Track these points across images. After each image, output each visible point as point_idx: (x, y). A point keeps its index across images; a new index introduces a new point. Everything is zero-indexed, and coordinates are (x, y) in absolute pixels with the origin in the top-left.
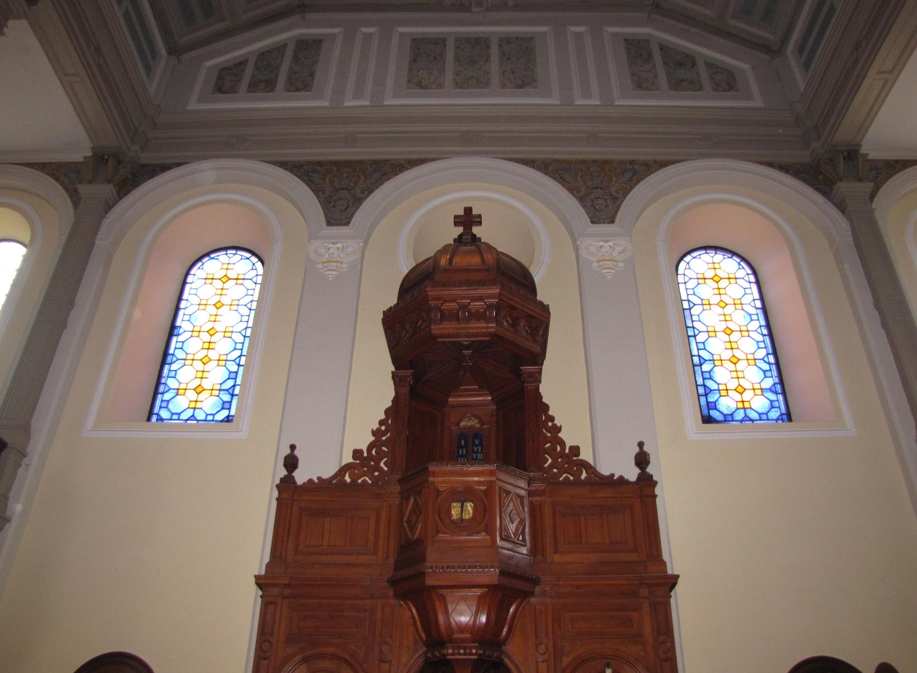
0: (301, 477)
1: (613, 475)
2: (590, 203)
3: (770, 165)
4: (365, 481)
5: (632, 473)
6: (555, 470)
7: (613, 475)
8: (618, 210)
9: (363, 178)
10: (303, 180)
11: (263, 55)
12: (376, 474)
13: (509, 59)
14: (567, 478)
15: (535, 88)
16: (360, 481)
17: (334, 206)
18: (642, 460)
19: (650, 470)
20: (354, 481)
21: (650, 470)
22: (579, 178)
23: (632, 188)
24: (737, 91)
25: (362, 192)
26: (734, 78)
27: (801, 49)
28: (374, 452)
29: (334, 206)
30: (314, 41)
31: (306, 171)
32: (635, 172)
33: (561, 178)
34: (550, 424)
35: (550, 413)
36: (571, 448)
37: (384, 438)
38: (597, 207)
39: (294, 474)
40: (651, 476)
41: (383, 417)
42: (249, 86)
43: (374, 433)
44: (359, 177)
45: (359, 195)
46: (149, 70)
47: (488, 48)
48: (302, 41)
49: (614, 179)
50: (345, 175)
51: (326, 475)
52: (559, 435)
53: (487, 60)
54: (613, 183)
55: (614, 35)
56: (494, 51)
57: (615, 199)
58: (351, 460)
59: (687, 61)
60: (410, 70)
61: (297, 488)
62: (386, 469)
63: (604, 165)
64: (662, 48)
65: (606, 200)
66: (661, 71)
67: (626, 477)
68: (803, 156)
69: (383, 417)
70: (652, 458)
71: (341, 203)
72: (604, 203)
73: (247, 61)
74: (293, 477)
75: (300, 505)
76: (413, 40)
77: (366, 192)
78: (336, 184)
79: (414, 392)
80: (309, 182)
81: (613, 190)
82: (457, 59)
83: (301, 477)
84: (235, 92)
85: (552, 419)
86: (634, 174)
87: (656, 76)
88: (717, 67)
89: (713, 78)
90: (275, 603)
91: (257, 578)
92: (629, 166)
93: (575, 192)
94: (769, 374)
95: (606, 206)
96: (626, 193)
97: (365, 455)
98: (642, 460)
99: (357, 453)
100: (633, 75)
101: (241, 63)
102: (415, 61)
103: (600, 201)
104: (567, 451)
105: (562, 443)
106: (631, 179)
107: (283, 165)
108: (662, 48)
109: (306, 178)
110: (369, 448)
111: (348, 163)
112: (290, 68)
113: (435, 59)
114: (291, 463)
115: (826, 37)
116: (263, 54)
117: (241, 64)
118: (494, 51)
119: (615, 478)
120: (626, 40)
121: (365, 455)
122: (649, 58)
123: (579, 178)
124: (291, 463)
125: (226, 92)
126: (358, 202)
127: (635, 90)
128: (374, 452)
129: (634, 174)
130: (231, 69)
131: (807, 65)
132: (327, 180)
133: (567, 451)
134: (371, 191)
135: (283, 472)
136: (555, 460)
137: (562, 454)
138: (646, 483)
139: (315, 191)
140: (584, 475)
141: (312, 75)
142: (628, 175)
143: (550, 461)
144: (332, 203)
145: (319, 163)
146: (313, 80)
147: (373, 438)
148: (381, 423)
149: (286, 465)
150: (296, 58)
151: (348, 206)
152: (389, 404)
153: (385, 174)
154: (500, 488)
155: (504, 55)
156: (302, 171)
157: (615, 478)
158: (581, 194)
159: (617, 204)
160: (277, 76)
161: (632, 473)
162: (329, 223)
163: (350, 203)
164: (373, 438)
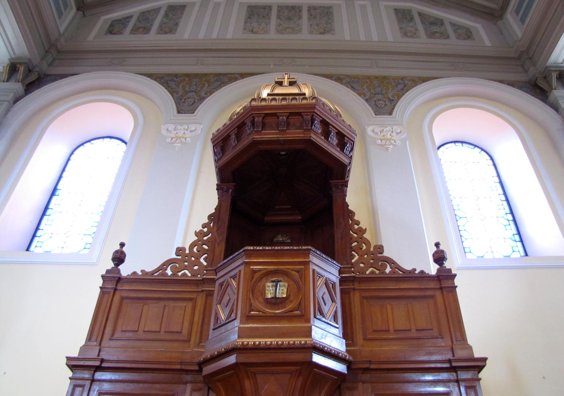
0: (125, 270)
1: (415, 270)
2: (374, 103)
3: (501, 82)
4: (184, 274)
5: (433, 269)
6: (362, 265)
7: (415, 270)
8: (394, 109)
9: (207, 85)
10: (164, 86)
11: (143, 13)
12: (196, 268)
13: (315, 18)
14: (372, 272)
15: (333, 34)
16: (180, 274)
17: (184, 102)
18: (440, 258)
19: (447, 265)
20: (174, 274)
21: (447, 265)
22: (365, 87)
23: (403, 94)
24: (474, 40)
25: (206, 94)
26: (471, 32)
27: (517, 12)
28: (195, 250)
29: (184, 102)
30: (180, 6)
31: (166, 80)
32: (405, 85)
33: (352, 87)
34: (356, 227)
35: (356, 218)
36: (375, 247)
37: (205, 238)
38: (379, 106)
39: (120, 267)
40: (450, 270)
41: (206, 221)
42: (132, 30)
43: (196, 234)
44: (205, 85)
45: (203, 94)
46: (60, 14)
47: (300, 11)
48: (172, 6)
49: (391, 89)
50: (194, 83)
51: (149, 268)
52: (365, 236)
53: (300, 17)
54: (390, 91)
55: (386, 6)
56: (305, 14)
57: (391, 101)
58: (174, 256)
59: (439, 22)
60: (246, 22)
61: (119, 280)
62: (205, 264)
63: (383, 79)
64: (420, 14)
65: (385, 101)
66: (420, 27)
67: (427, 271)
68: (522, 77)
69: (206, 221)
70: (448, 256)
71: (189, 100)
72: (384, 103)
73: (132, 16)
74: (119, 270)
75: (120, 292)
76: (249, 7)
77: (208, 94)
78: (187, 89)
79: (234, 204)
80: (168, 87)
81: (390, 96)
82: (279, 17)
83: (125, 270)
84: (121, 33)
85: (358, 223)
86: (405, 86)
87: (417, 30)
88: (459, 26)
89: (456, 32)
90: (83, 386)
91: (68, 359)
92: (400, 81)
93: (362, 96)
94: (508, 227)
95: (386, 105)
96: (399, 97)
97: (187, 252)
98: (440, 258)
99: (180, 251)
100: (401, 28)
101: (128, 17)
102: (249, 18)
103: (381, 102)
104: (372, 249)
105: (367, 243)
106: (402, 89)
107: (150, 76)
108: (420, 14)
109: (165, 85)
110: (192, 246)
111: (196, 75)
112: (162, 21)
113: (263, 17)
114: (119, 258)
115: (269, 341)
116: (144, 13)
117: (129, 18)
118: (305, 14)
119: (417, 272)
120: (395, 9)
121: (187, 252)
122: (412, 19)
123: (365, 87)
124: (119, 258)
125: (115, 34)
126: (202, 99)
127: (403, 37)
128: (195, 250)
129: (405, 86)
130: (120, 21)
131: (522, 20)
132: (181, 86)
133: (372, 249)
134: (212, 93)
135: (111, 265)
136: (361, 256)
137: (367, 252)
138: (445, 280)
139: (172, 93)
140: (388, 270)
141: (177, 25)
142: (401, 86)
143: (357, 257)
144: (183, 100)
145: (176, 75)
146: (177, 28)
147: (196, 238)
148: (204, 226)
149: (114, 259)
150: (166, 15)
151: (195, 102)
152: (213, 211)
153: (224, 83)
154: (314, 270)
155: (311, 15)
156: (163, 80)
157: (417, 272)
158: (367, 97)
159: (393, 105)
160: (152, 25)
161: (433, 269)
162: (179, 112)
163: (196, 100)
164: (196, 238)
